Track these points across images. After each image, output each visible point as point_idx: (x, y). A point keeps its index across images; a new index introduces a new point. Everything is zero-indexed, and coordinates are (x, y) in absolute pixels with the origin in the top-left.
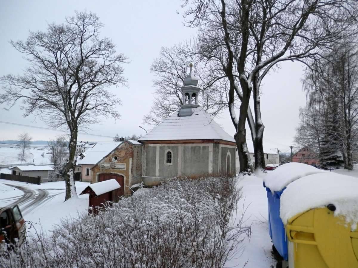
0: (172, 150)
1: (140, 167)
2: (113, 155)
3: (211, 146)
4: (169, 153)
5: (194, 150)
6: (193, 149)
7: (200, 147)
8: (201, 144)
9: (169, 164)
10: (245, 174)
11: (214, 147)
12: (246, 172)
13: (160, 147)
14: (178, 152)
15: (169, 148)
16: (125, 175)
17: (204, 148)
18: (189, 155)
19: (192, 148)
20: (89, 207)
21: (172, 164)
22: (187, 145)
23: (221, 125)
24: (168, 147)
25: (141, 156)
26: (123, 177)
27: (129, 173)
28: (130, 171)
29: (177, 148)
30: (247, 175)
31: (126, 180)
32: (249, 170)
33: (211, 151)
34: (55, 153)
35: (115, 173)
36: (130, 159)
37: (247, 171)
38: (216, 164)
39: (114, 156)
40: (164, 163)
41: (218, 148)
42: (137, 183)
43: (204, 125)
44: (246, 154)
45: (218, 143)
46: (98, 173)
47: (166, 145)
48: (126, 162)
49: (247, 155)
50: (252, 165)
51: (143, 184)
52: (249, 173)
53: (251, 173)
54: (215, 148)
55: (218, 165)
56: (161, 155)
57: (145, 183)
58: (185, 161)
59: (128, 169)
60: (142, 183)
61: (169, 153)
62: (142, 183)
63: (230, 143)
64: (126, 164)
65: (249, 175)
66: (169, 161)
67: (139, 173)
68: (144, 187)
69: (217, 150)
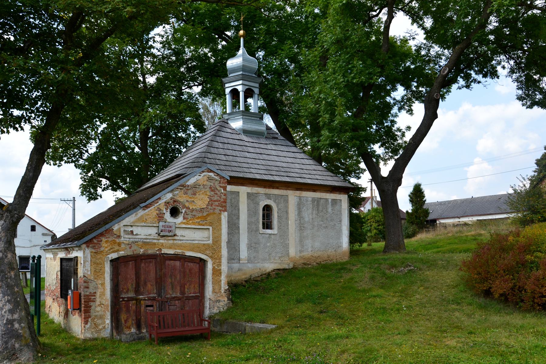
0: (275, 201)
2: (167, 203)
4: (267, 209)
5: (318, 205)
6: (316, 202)
7: (327, 200)
9: (269, 231)
13: (249, 195)
14: (287, 207)
15: (268, 196)
16: (211, 257)
17: (334, 202)
18: (308, 214)
19: (313, 200)
20: (493, 298)
21: (275, 231)
22: (305, 194)
26: (202, 263)
27: (220, 252)
28: (224, 245)
29: (286, 199)
31: (214, 268)
34: (340, 168)
35: (179, 251)
36: (223, 217)
39: (170, 207)
46: (114, 256)
47: (261, 190)
48: (211, 224)
56: (252, 213)
58: (301, 227)
59: (217, 241)
61: (267, 209)
64: (211, 228)
66: (267, 225)
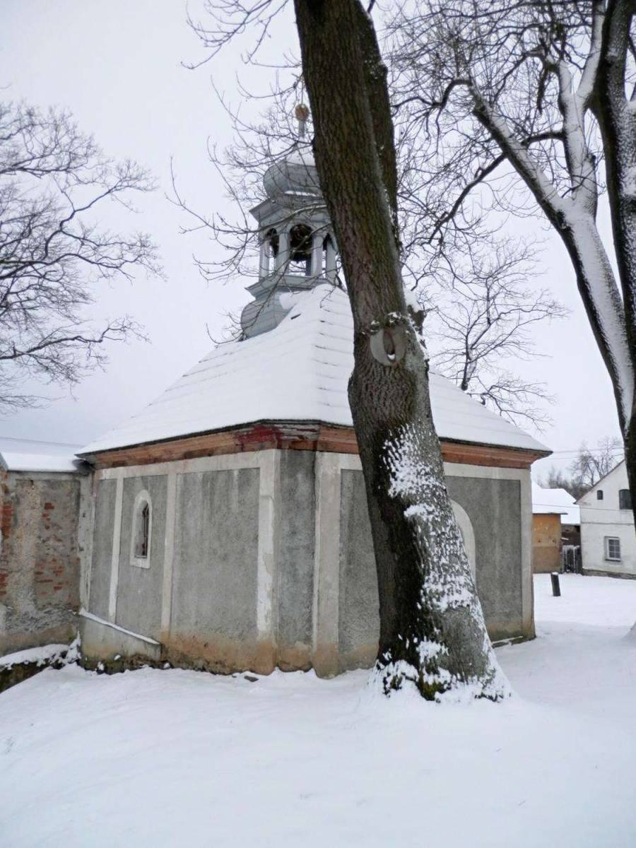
1: (68, 570)
3: (267, 461)
8: (232, 456)
10: (396, 685)
11: (287, 470)
12: (403, 667)
23: (542, 386)
24: (241, 487)
25: (75, 522)
30: (409, 688)
32: (428, 649)
33: (266, 497)
37: (413, 659)
38: (294, 575)
40: (129, 559)
41: (312, 473)
42: (42, 645)
43: (100, 341)
44: (410, 512)
45: (315, 447)
49: (415, 521)
50: (463, 609)
51: (79, 649)
52: (429, 679)
53: (445, 675)
54: (293, 476)
55: (311, 585)
57: (85, 649)
58: (184, 557)
60: (77, 642)
62: (74, 644)
63: (503, 456)
65: (428, 692)
67: (61, 596)
68: (78, 662)
69: (304, 488)
